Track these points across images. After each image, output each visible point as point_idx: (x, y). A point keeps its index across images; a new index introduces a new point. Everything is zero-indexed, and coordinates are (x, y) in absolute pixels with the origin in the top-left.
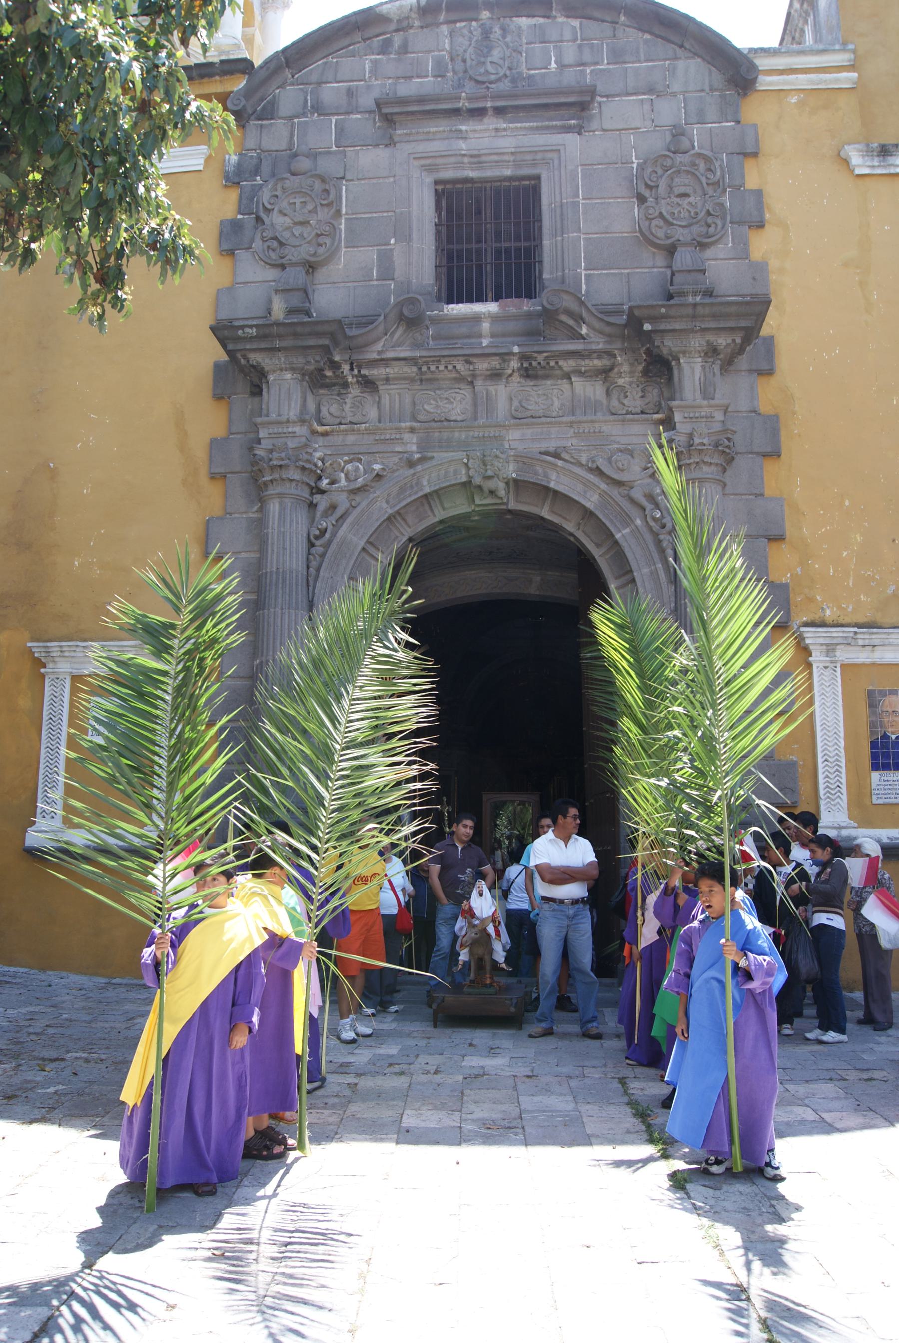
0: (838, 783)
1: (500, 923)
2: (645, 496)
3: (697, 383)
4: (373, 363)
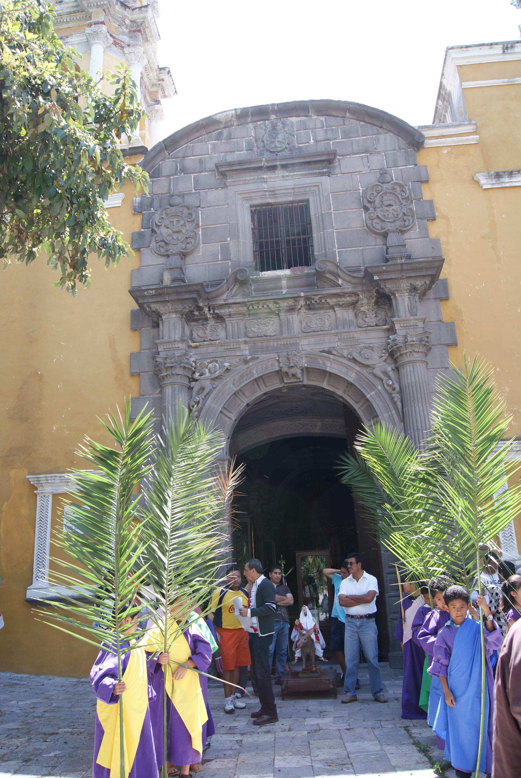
0: (510, 534)
1: (318, 632)
2: (382, 372)
3: (407, 307)
4: (221, 306)
